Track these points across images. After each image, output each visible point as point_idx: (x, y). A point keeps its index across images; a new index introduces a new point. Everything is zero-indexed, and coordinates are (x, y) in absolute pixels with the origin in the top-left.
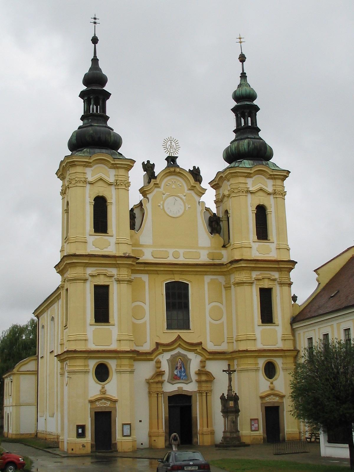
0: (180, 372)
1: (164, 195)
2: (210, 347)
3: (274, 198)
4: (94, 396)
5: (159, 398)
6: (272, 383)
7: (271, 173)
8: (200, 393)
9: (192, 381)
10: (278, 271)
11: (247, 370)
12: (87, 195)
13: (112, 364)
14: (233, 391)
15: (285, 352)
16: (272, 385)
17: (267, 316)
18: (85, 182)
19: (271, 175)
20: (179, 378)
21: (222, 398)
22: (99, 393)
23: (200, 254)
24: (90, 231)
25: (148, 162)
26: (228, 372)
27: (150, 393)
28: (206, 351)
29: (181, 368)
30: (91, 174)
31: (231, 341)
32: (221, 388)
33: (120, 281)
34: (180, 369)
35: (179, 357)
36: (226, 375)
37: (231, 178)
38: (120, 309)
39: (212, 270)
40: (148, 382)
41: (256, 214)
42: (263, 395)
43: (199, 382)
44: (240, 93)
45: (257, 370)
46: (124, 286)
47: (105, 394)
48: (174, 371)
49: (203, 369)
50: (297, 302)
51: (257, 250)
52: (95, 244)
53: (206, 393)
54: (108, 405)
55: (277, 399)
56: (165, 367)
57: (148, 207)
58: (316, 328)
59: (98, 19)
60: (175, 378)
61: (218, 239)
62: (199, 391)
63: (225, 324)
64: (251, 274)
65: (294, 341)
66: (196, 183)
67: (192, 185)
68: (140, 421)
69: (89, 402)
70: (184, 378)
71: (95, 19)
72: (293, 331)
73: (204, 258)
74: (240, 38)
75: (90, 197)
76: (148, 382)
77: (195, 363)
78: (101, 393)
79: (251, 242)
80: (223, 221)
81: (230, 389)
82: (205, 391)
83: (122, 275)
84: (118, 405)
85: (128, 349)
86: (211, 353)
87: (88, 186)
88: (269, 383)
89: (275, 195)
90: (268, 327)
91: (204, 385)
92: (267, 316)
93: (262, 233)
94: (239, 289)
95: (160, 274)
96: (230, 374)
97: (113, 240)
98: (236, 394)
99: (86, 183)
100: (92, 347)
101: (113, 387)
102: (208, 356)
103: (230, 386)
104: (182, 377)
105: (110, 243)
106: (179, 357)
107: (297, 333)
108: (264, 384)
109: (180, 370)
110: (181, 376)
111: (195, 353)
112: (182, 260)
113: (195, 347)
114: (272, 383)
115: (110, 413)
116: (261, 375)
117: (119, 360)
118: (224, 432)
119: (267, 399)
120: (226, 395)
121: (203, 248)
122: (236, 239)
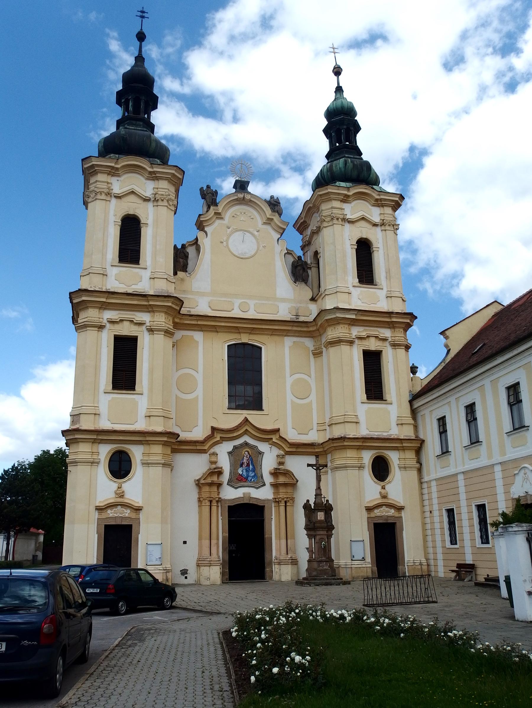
0: (247, 471)
1: (229, 228)
2: (292, 435)
3: (382, 231)
4: (105, 501)
5: (212, 507)
6: (383, 488)
7: (378, 197)
8: (276, 502)
9: (264, 485)
10: (390, 328)
11: (345, 467)
12: (112, 213)
13: (137, 453)
14: (323, 496)
15: (403, 441)
16: (383, 491)
17: (374, 389)
18: (109, 194)
19: (377, 200)
20: (246, 479)
21: (307, 506)
22: (113, 495)
23: (278, 307)
24: (113, 259)
25: (208, 187)
26: (315, 468)
27: (199, 501)
28: (286, 440)
29: (248, 465)
30: (118, 185)
31: (322, 428)
32: (306, 493)
33: (153, 331)
34: (247, 466)
35: (246, 450)
36: (312, 472)
37: (321, 203)
38: (151, 371)
39: (295, 328)
40: (199, 484)
41: (357, 250)
42: (371, 505)
43: (275, 486)
44: (335, 106)
45: (361, 467)
46: (160, 338)
47: (122, 496)
48: (238, 470)
49: (281, 467)
50: (418, 375)
51: (360, 298)
52: (120, 278)
53: (286, 502)
54: (127, 515)
55: (392, 512)
56: (224, 463)
57: (205, 243)
58: (452, 399)
59: (147, 13)
60: (237, 480)
61: (306, 292)
62: (276, 498)
63: (314, 406)
64: (350, 330)
65: (416, 427)
66: (274, 214)
67: (268, 216)
68: (185, 542)
69: (96, 509)
70: (253, 480)
71: (143, 12)
72: (414, 412)
73: (284, 313)
74: (334, 49)
75: (115, 215)
76: (199, 484)
77: (269, 460)
78: (117, 496)
79: (350, 286)
80: (312, 268)
81: (318, 494)
82: (283, 499)
83: (157, 323)
84: (142, 516)
85: (160, 429)
86: (292, 445)
87: (114, 200)
88: (379, 487)
89: (383, 227)
90: (376, 406)
91: (282, 490)
92: (374, 389)
93: (366, 274)
94: (332, 350)
95: (220, 332)
96: (318, 469)
97: (146, 275)
98: (327, 501)
99: (111, 196)
100: (105, 424)
101: (134, 488)
102: (289, 448)
103: (319, 488)
104: (249, 479)
105: (141, 277)
106: (246, 450)
107: (419, 416)
108: (372, 490)
109: (246, 467)
110: (248, 476)
111: (270, 444)
112: (251, 314)
113: (269, 435)
114: (383, 488)
115: (129, 528)
116: (367, 474)
117: (147, 447)
118: (309, 561)
119: (376, 511)
120: (312, 503)
121: (283, 300)
122: (329, 282)
